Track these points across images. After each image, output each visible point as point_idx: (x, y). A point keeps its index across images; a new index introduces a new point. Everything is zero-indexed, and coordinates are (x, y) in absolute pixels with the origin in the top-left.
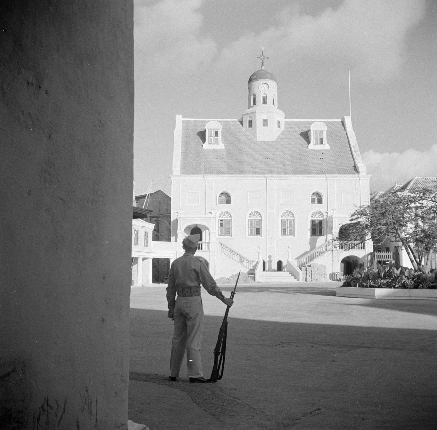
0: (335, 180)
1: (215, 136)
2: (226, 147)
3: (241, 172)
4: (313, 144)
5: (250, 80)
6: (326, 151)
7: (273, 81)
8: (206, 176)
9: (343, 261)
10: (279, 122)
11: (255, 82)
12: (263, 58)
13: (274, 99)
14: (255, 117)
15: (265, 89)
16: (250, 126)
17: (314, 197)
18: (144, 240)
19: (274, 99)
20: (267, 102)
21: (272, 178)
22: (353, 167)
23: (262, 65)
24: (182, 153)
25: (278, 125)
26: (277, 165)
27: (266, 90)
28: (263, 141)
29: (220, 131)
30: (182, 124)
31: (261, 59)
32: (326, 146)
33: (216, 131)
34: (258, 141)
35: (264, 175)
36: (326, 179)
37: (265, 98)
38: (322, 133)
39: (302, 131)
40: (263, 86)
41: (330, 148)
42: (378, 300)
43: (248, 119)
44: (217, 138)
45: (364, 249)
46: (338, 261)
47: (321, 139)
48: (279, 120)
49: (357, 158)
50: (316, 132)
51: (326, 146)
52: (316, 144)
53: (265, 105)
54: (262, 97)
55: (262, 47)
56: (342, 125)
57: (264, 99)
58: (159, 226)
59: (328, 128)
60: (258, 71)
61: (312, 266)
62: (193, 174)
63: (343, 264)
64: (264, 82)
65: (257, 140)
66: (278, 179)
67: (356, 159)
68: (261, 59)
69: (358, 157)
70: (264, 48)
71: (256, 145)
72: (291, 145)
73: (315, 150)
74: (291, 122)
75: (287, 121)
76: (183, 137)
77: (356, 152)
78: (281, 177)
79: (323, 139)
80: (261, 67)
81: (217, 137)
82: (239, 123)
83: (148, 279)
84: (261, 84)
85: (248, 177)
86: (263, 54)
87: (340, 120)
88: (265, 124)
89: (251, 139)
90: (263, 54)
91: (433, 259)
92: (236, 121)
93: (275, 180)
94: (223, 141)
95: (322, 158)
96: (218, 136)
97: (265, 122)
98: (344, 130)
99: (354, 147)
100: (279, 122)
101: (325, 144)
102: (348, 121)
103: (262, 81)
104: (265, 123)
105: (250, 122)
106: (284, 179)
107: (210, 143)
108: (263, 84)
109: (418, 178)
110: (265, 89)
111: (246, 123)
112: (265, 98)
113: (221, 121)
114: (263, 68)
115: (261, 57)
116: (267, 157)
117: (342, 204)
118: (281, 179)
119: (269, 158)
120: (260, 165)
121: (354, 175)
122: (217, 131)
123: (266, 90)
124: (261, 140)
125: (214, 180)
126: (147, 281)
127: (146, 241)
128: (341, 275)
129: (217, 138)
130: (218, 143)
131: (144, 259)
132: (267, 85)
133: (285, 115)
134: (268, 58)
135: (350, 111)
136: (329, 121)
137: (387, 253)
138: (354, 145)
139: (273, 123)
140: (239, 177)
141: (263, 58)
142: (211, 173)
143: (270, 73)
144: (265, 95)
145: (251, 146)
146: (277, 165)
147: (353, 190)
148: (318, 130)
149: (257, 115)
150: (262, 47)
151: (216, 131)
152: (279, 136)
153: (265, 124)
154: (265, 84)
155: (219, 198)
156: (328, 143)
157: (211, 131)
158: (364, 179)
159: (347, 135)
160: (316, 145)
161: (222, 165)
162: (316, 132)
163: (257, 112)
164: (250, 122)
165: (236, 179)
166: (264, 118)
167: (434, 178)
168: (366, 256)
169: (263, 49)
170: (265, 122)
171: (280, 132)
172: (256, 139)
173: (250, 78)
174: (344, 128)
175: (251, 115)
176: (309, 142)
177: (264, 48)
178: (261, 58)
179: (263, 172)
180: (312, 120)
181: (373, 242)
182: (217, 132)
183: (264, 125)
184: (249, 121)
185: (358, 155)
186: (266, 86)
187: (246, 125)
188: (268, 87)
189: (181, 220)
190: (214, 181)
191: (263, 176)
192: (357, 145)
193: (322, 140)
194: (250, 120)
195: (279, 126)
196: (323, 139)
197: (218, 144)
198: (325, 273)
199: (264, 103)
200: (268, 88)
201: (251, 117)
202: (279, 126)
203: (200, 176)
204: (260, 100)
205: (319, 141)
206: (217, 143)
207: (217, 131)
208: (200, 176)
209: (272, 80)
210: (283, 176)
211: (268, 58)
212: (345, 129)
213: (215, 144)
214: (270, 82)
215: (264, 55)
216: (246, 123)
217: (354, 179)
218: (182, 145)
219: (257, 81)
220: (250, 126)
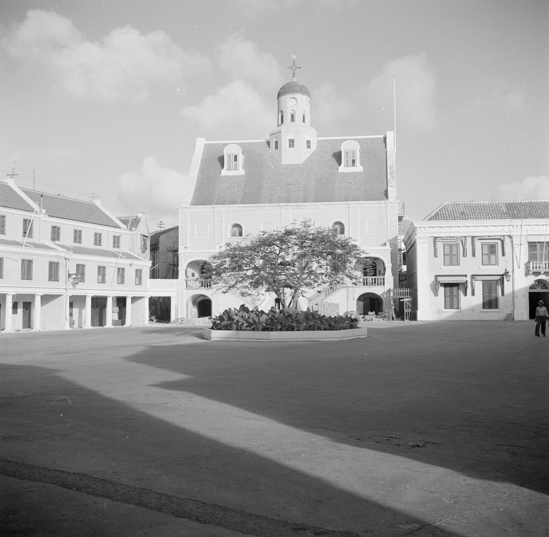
0: (358, 208)
1: (234, 161)
2: (246, 173)
3: (256, 201)
4: (344, 166)
5: (279, 95)
6: (360, 173)
7: (303, 95)
8: (215, 207)
9: (360, 299)
10: (308, 142)
11: (282, 97)
12: (294, 68)
13: (304, 116)
14: (280, 136)
15: (293, 104)
16: (276, 147)
17: (337, 226)
18: (135, 278)
19: (304, 116)
20: (296, 120)
21: (287, 207)
22: (385, 191)
23: (294, 76)
24: (197, 181)
25: (307, 145)
26: (298, 192)
27: (295, 105)
28: (288, 165)
29: (239, 155)
30: (204, 148)
31: (292, 69)
32: (359, 168)
33: (235, 156)
34: (282, 165)
35: (278, 204)
36: (348, 206)
37: (293, 115)
38: (354, 152)
39: (335, 151)
40: (291, 101)
41: (364, 169)
42: (348, 341)
43: (275, 140)
44: (237, 163)
45: (384, 285)
46: (354, 299)
47: (353, 160)
48: (309, 139)
49: (391, 181)
50: (347, 153)
51: (359, 168)
52: (347, 165)
53: (293, 123)
54: (289, 113)
55: (292, 55)
56: (384, 142)
57: (292, 116)
58: (491, 258)
59: (361, 147)
60: (286, 84)
61: (318, 305)
62: (204, 205)
63: (362, 303)
64: (292, 96)
65: (283, 164)
66: (293, 208)
67: (389, 182)
68: (292, 69)
69: (392, 180)
70: (295, 56)
71: (280, 169)
72: (319, 168)
73: (345, 173)
74: (326, 141)
75: (320, 140)
76: (202, 163)
77: (391, 173)
78: (297, 205)
79: (355, 160)
80: (292, 78)
81: (236, 162)
82: (266, 144)
83: (144, 319)
84: (288, 99)
85: (261, 206)
86: (294, 63)
87: (382, 136)
88: (292, 145)
89: (276, 163)
90: (294, 63)
91: (455, 296)
92: (263, 142)
93: (290, 210)
94: (245, 167)
95: (351, 182)
96: (238, 161)
97: (292, 143)
98: (385, 148)
99: (390, 168)
100: (308, 142)
101: (357, 165)
102: (391, 137)
103: (289, 95)
104: (291, 143)
105: (276, 143)
106: (301, 208)
107: (229, 169)
108: (291, 99)
109: (448, 203)
110: (293, 104)
111: (273, 145)
112: (293, 115)
113: (239, 143)
114: (294, 80)
115: (295, 69)
116: (289, 183)
117: (367, 234)
118: (298, 208)
119: (291, 183)
120: (279, 193)
121: (380, 201)
122: (237, 155)
123: (295, 105)
124: (287, 164)
125: (224, 211)
126: (144, 321)
127: (137, 279)
128: (355, 316)
129: (237, 163)
130: (238, 169)
131: (134, 299)
132: (295, 100)
133: (316, 133)
134: (300, 68)
135: (395, 124)
136: (369, 138)
137: (399, 289)
138: (392, 165)
139: (300, 144)
140: (251, 207)
141: (294, 68)
142: (223, 203)
143: (300, 86)
144: (294, 112)
145: (274, 171)
146: (298, 192)
147: (379, 218)
148: (350, 150)
149: (282, 135)
150: (292, 55)
151: (235, 156)
152: (308, 158)
153: (292, 145)
154: (293, 99)
155: (231, 230)
156: (362, 165)
157: (229, 156)
158: (392, 205)
159: (386, 153)
160: (347, 166)
161: (237, 194)
162: (347, 153)
163: (282, 131)
164: (276, 143)
165: (248, 209)
166: (290, 138)
167: (468, 203)
168: (385, 293)
169: (295, 57)
170: (292, 143)
171: (310, 154)
172: (281, 160)
173: (279, 92)
174: (384, 146)
175: (276, 135)
176: (340, 164)
177: (295, 56)
178: (296, 68)
179: (280, 200)
180: (344, 138)
181: (393, 277)
182: (236, 157)
183: (290, 146)
184: (275, 142)
185: (393, 177)
186: (294, 101)
187: (273, 147)
188: (296, 102)
189: (183, 256)
190: (224, 213)
191: (277, 205)
192: (395, 165)
193: (354, 161)
194: (276, 140)
195: (309, 147)
196: (355, 160)
197: (237, 170)
198: (337, 311)
199: (292, 121)
200: (296, 104)
201: (276, 137)
202: (309, 147)
203: (209, 207)
204: (287, 118)
205: (350, 163)
206: (236, 169)
207: (237, 155)
208: (209, 207)
209: (301, 94)
210: (299, 205)
211: (300, 68)
212: (386, 147)
213: (234, 170)
214: (299, 96)
215: (295, 64)
216: (273, 145)
217: (380, 205)
218: (199, 172)
219: (284, 96)
220: (276, 147)
